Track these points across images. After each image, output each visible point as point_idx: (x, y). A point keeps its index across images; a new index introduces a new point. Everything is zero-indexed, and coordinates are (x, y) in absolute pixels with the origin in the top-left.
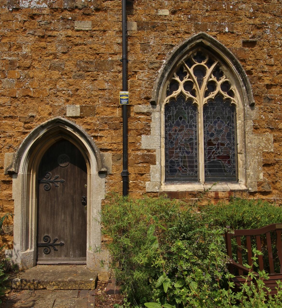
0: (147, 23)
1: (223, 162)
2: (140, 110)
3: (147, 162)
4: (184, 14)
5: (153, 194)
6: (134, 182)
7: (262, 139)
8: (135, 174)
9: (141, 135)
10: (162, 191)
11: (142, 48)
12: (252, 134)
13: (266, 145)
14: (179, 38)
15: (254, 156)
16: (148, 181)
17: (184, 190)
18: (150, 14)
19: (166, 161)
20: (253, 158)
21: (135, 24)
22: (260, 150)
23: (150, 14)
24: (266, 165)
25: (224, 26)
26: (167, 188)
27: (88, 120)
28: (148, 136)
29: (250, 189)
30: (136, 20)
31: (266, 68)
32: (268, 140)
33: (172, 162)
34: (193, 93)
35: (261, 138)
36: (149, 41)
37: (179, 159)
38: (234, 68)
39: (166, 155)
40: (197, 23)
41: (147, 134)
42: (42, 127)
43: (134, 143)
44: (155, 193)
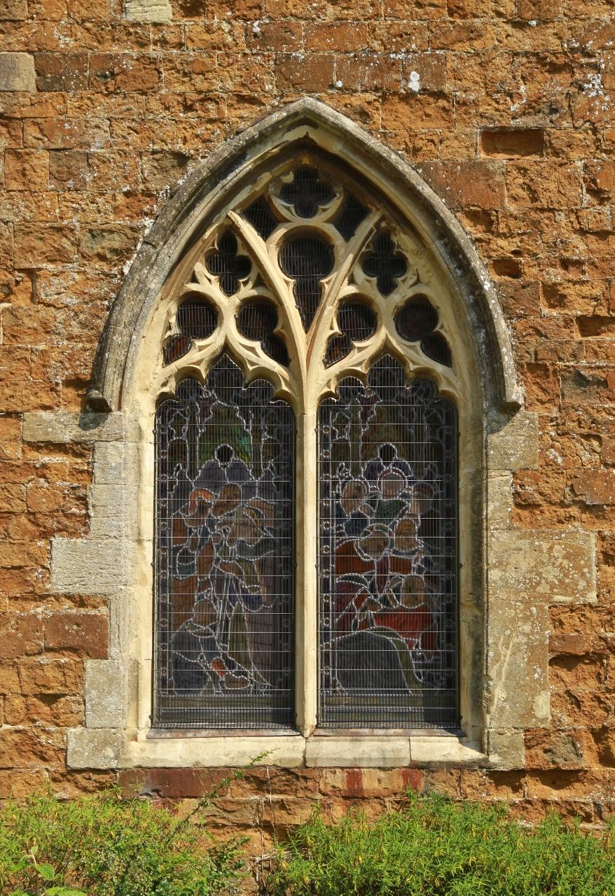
0: (78, 59)
1: (403, 640)
2: (47, 433)
3: (73, 650)
4: (236, 18)
5: (94, 777)
6: (21, 727)
7: (551, 548)
8: (25, 696)
9: (46, 534)
10: (129, 765)
11: (54, 168)
12: (509, 529)
13: (566, 576)
14: (211, 121)
15: (513, 620)
16: (75, 726)
17: (223, 761)
18: (88, 20)
20: (508, 632)
21: (27, 63)
22: (542, 595)
23: (88, 20)
25: (404, 67)
26: (154, 752)
28: (79, 541)
29: (494, 759)
30: (34, 47)
32: (574, 555)
33: (183, 642)
34: (280, 349)
35: (545, 546)
36: (87, 138)
37: (214, 628)
38: (438, 247)
39: (161, 610)
40: (288, 57)
41: (73, 534)
43: (20, 568)
44: (105, 772)
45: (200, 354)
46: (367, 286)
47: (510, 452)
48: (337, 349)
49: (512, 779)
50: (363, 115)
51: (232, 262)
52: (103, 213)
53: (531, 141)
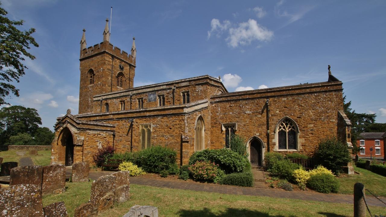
19: (279, 144)
24: (302, 146)
27: (261, 136)
31: (303, 123)
42: (252, 138)
45: (280, 130)
46: (290, 126)
47: (299, 134)
48: (288, 129)
49: (299, 152)
50: (290, 117)
51: (282, 125)
52: (275, 122)
53: (300, 118)
